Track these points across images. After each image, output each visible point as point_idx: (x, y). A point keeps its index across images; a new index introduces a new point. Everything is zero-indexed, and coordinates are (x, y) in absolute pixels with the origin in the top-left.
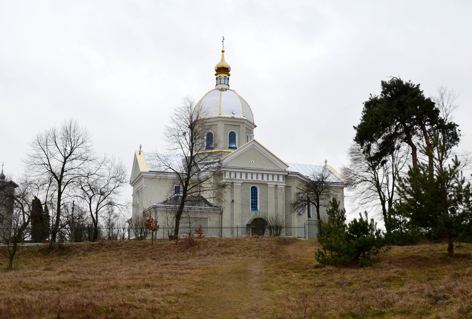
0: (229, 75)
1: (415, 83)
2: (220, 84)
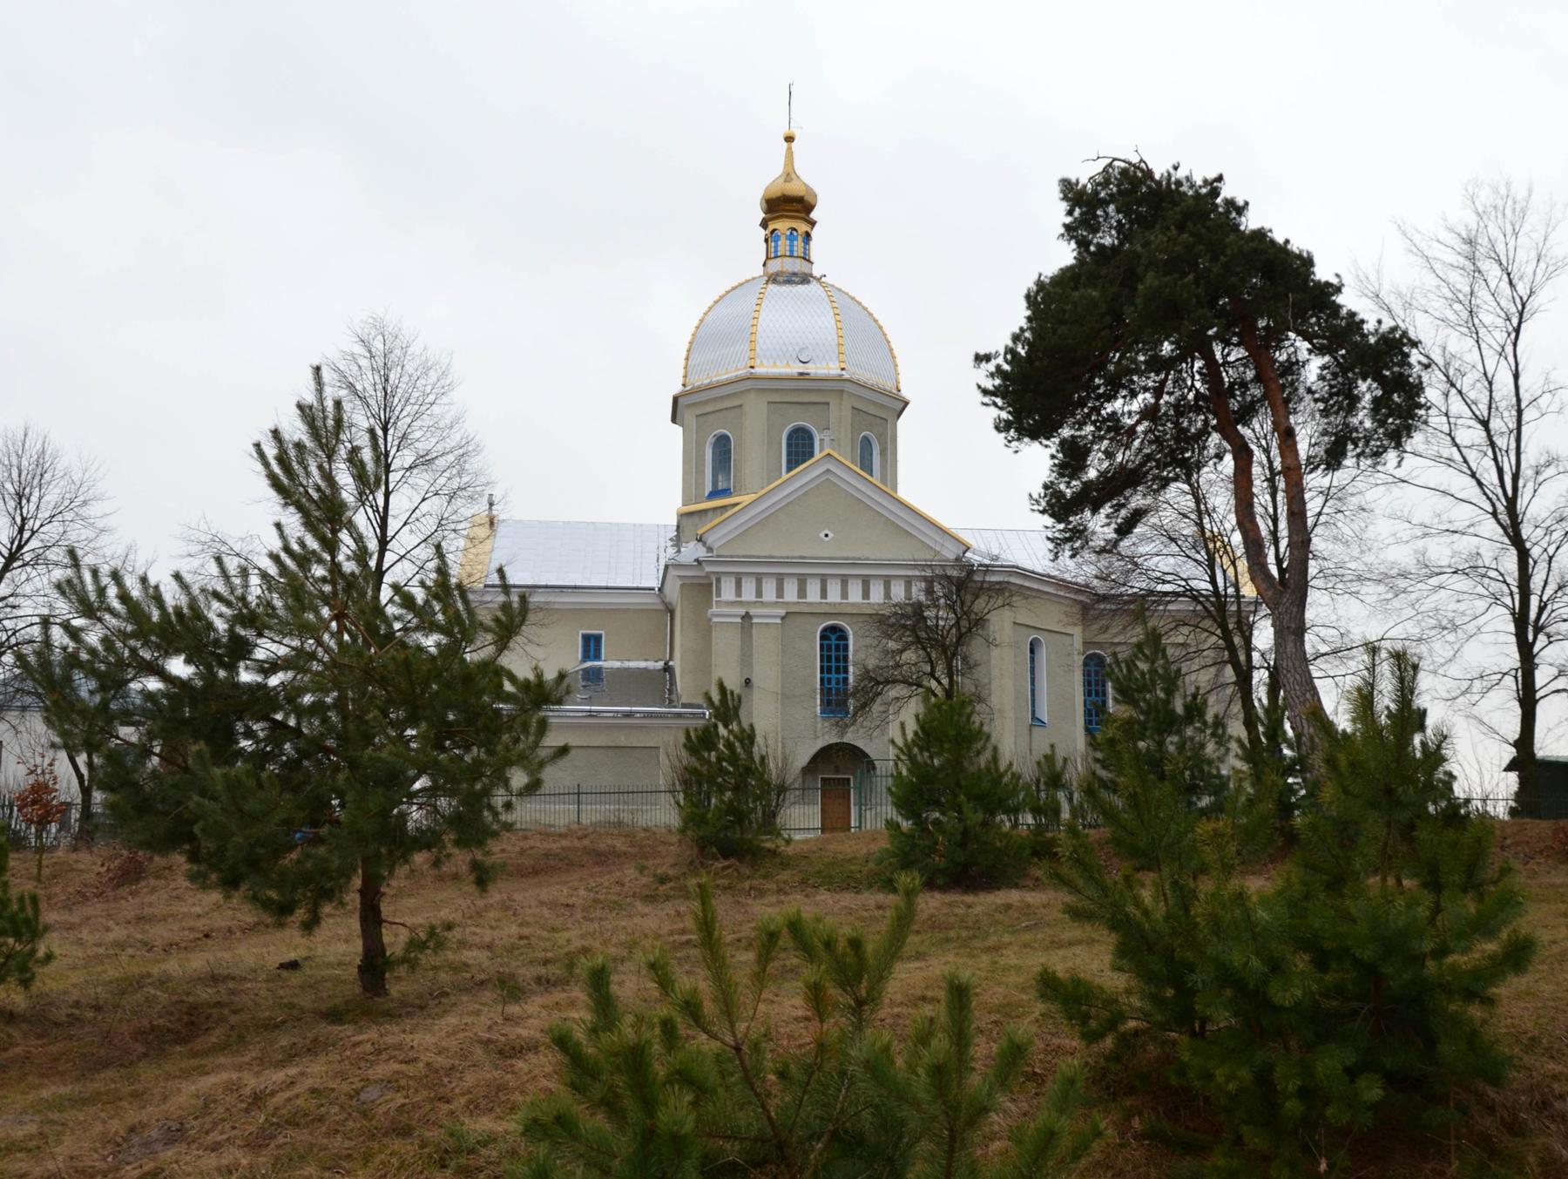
0: (813, 223)
1: (1198, 170)
2: (776, 257)
